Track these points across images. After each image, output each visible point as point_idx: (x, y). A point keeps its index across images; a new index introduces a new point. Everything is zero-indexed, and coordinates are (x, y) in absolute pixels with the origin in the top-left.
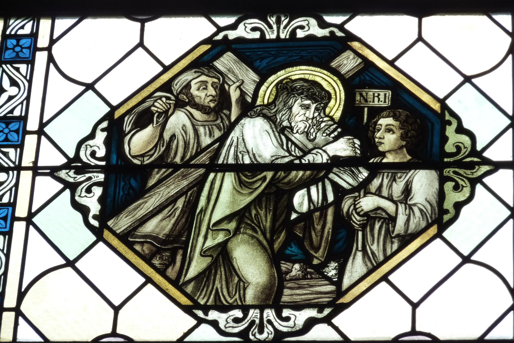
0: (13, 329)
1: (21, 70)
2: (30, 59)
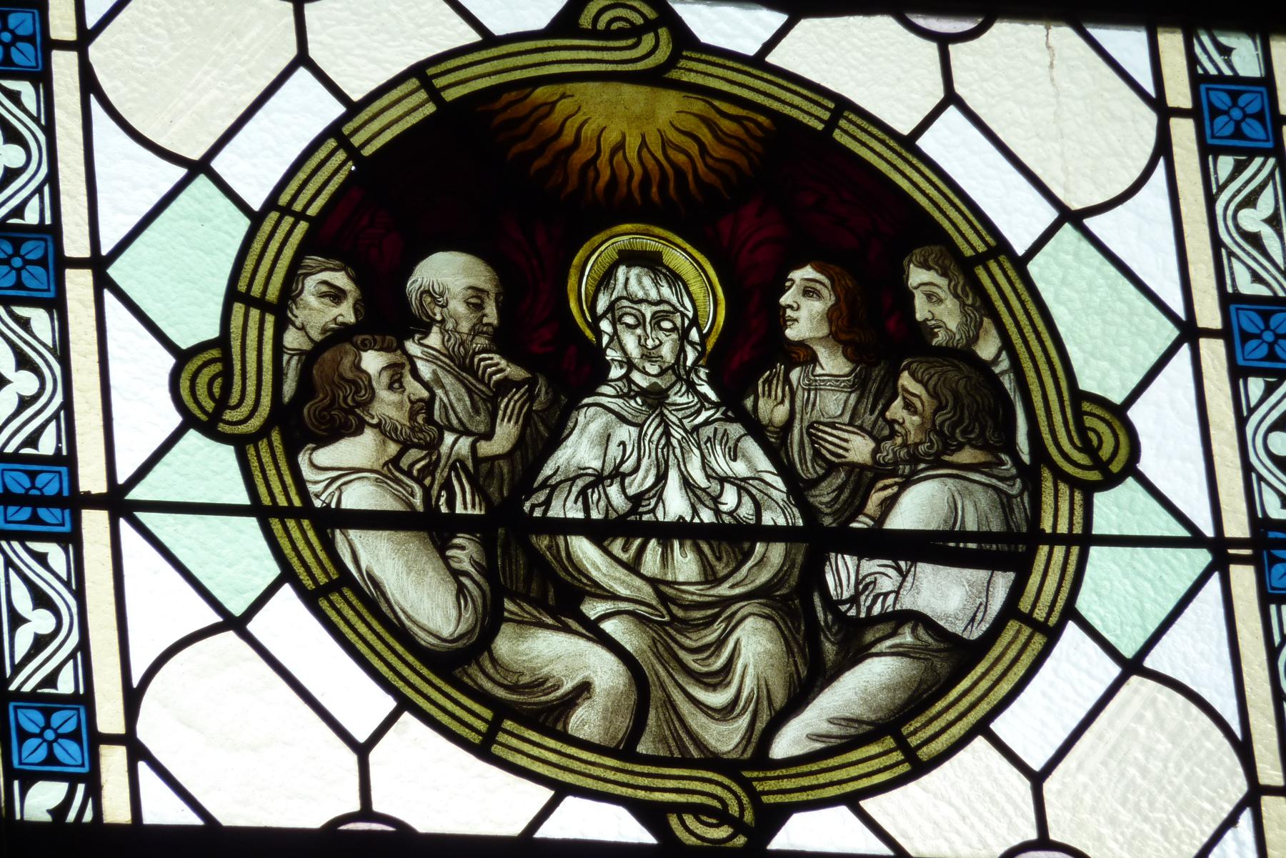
0: (126, 774)
1: (51, 561)
2: (40, 69)
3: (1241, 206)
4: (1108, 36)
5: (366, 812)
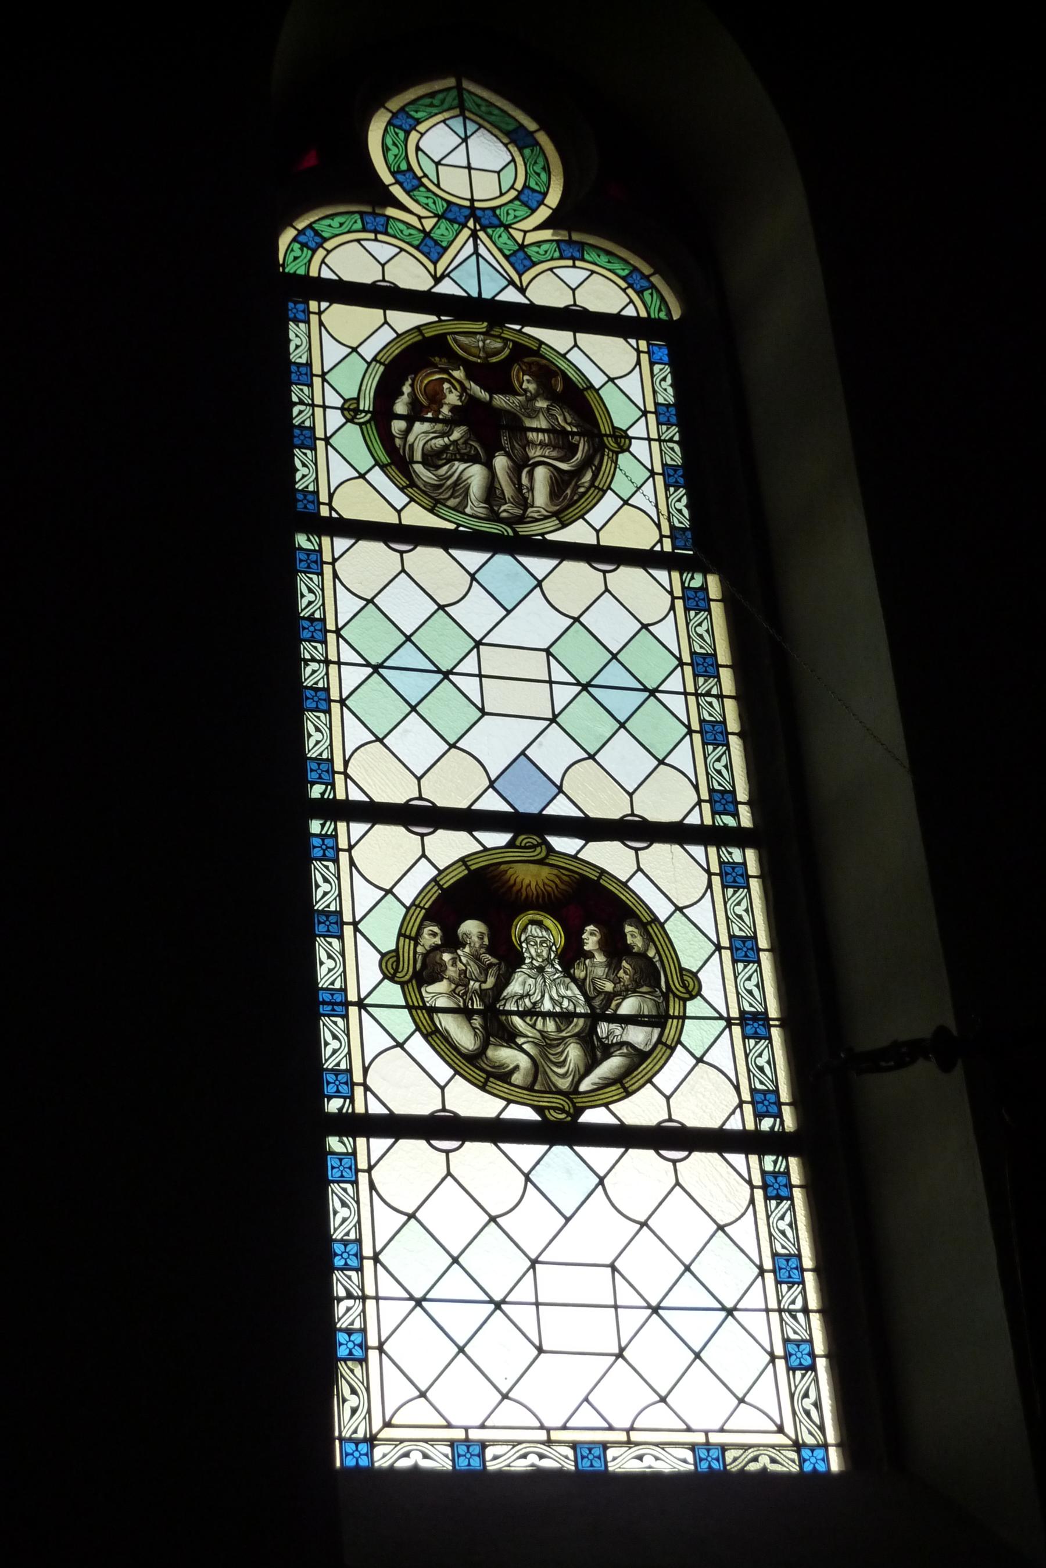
1: (338, 1024)
3: (716, 761)
5: (444, 1109)
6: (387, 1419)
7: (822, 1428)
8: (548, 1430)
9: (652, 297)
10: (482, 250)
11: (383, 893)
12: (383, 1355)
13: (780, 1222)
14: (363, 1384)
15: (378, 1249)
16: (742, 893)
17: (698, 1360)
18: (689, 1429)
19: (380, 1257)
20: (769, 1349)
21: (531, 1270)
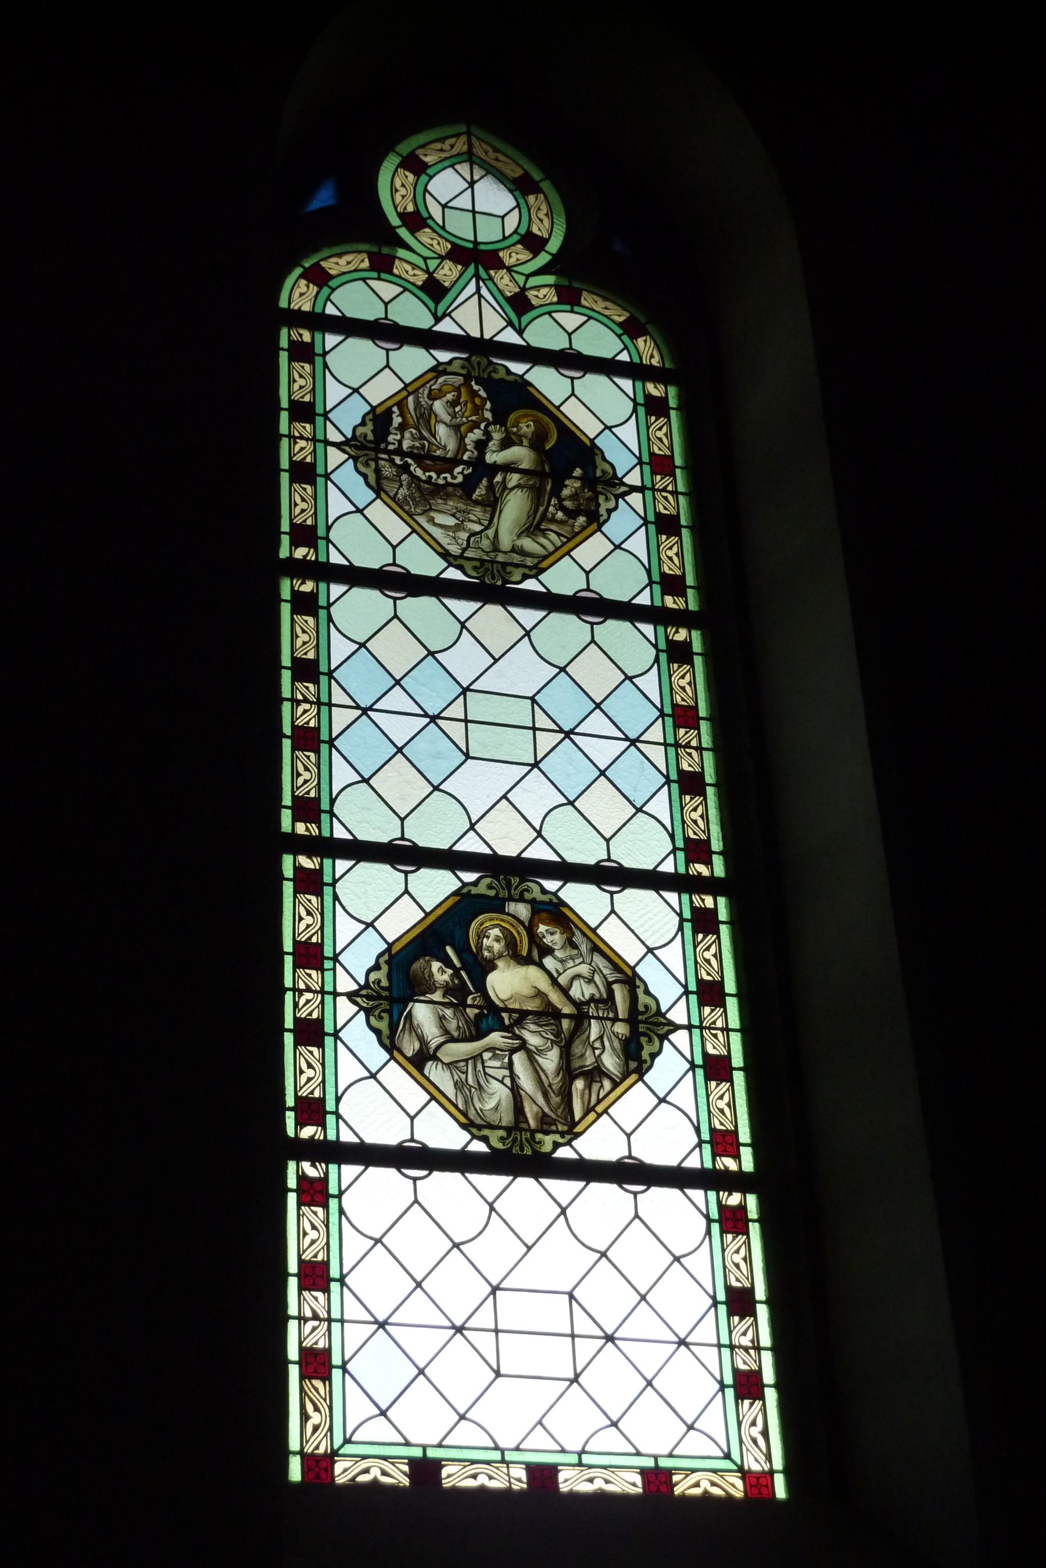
1: (307, 490)
3: (692, 811)
4: (666, 895)
5: (403, 838)
6: (348, 1436)
7: (769, 1457)
8: (502, 1451)
9: (645, 345)
10: (484, 291)
11: (364, 926)
12: (345, 1288)
13: (719, 1101)
14: (318, 911)
15: (346, 1358)
16: (711, 938)
17: (649, 1387)
18: (638, 1454)
19: (340, 958)
20: (705, 1211)
21: (492, 1296)
